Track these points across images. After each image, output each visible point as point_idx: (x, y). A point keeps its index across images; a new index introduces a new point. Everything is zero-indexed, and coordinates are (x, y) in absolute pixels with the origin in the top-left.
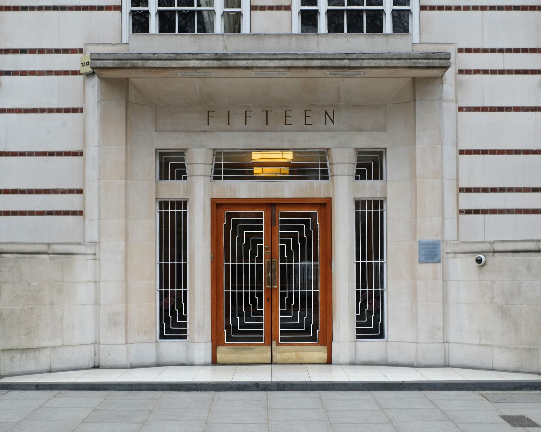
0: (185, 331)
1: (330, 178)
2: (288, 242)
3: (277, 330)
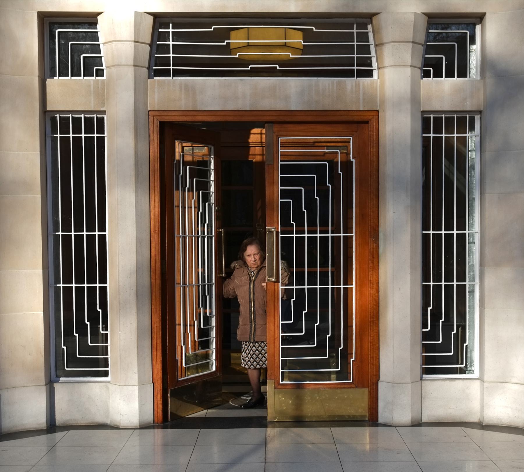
0: (106, 363)
1: (375, 73)
2: (295, 195)
3: (275, 338)
